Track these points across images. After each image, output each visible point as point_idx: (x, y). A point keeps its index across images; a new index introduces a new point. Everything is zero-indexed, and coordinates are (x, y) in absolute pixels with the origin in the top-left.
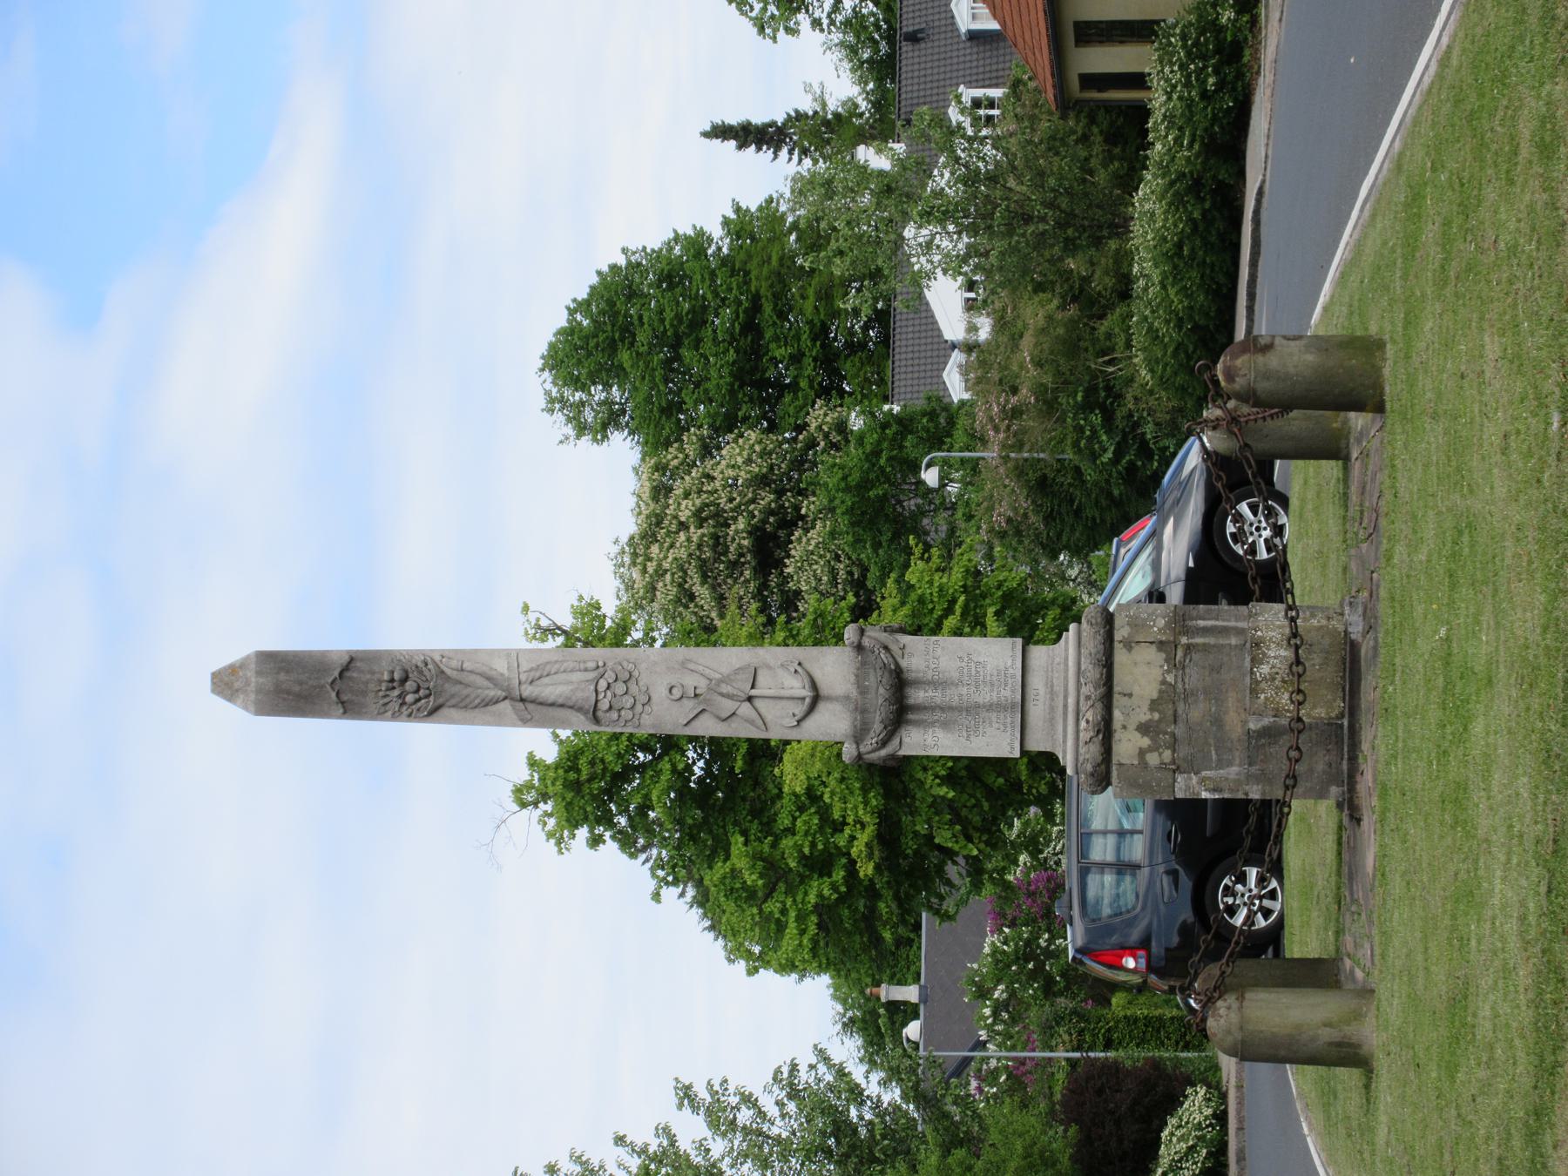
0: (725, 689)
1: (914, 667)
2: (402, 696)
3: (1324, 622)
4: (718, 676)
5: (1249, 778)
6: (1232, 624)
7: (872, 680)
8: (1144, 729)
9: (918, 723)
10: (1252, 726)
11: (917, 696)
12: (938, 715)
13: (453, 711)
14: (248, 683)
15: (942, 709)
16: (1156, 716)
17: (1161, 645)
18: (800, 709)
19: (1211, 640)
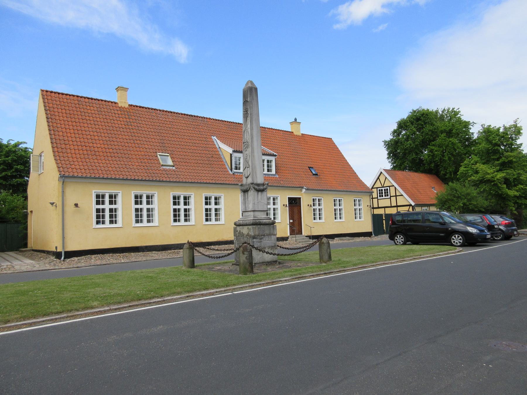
7: (247, 186)
11: (246, 193)
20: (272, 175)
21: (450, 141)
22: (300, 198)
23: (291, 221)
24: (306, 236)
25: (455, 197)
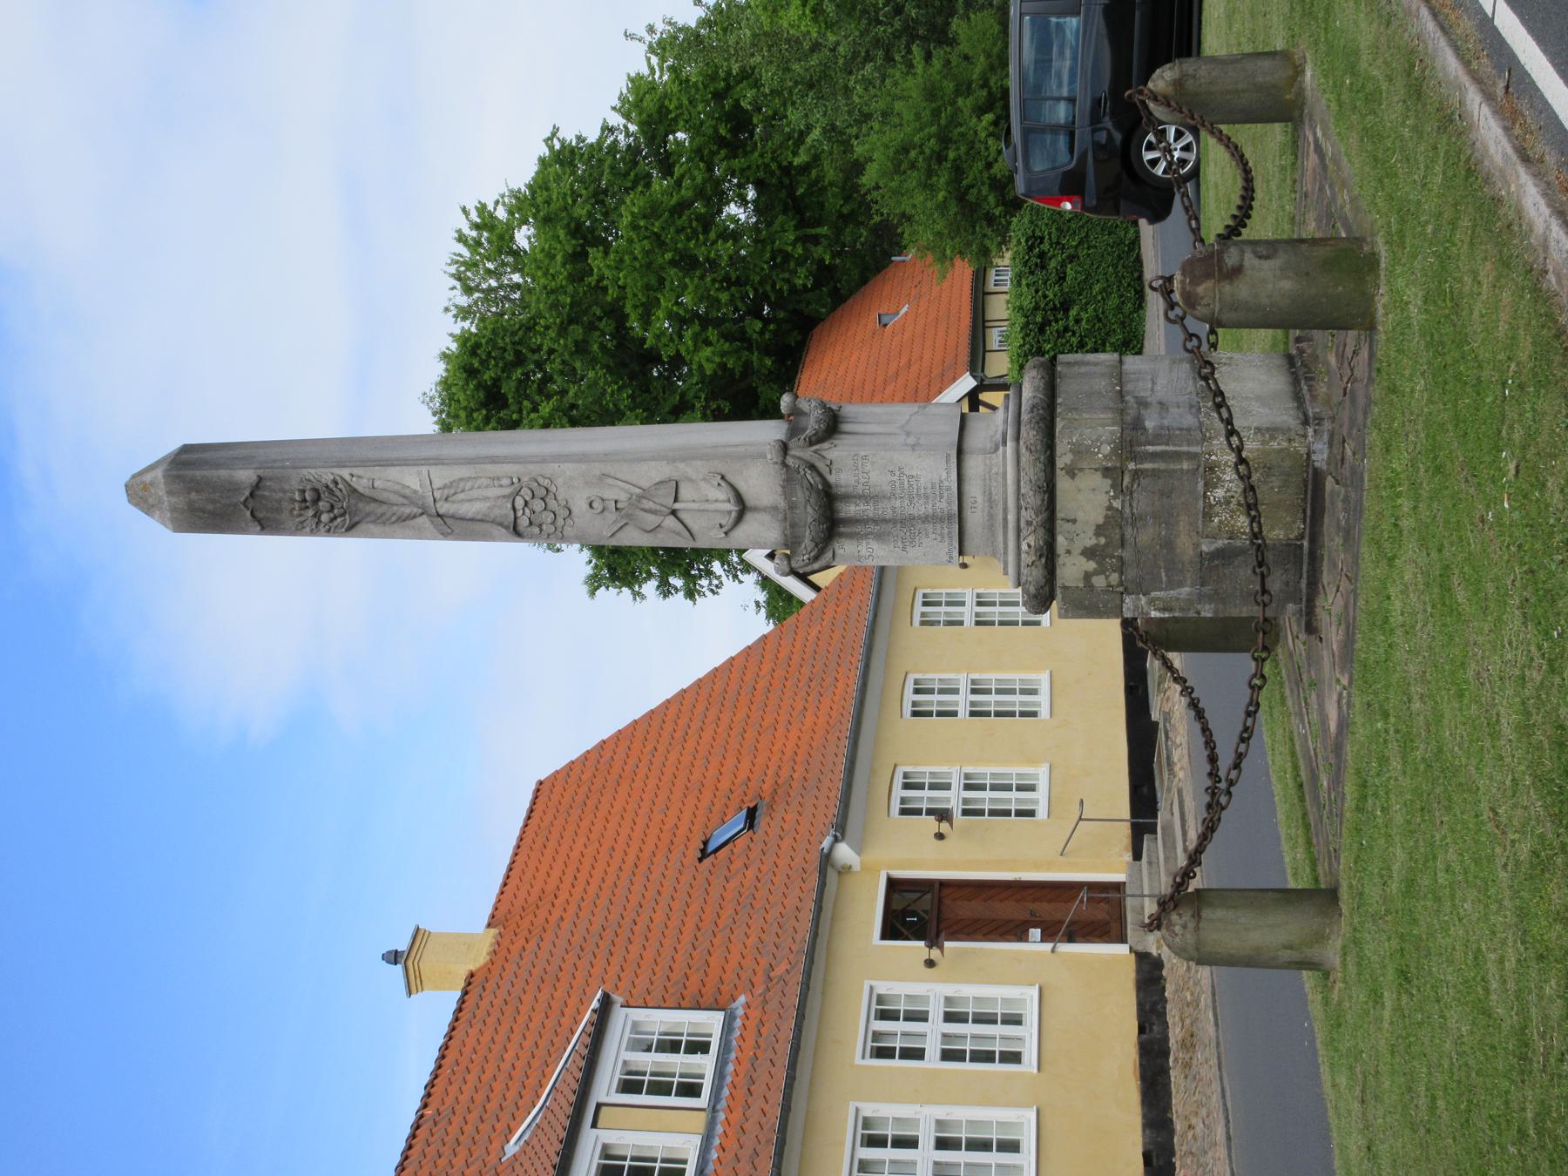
0: (648, 504)
1: (843, 482)
2: (317, 515)
3: (1285, 444)
4: (638, 491)
5: (1201, 598)
6: (1185, 449)
7: (800, 496)
8: (1089, 553)
9: (850, 536)
10: (1205, 548)
11: (849, 510)
12: (871, 528)
13: (372, 526)
14: (160, 501)
15: (875, 521)
16: (1103, 541)
17: (1107, 472)
18: (727, 521)
19: (1161, 466)
20: (727, 1028)
21: (634, 227)
22: (893, 885)
23: (1036, 933)
24: (1137, 856)
25: (940, 158)
